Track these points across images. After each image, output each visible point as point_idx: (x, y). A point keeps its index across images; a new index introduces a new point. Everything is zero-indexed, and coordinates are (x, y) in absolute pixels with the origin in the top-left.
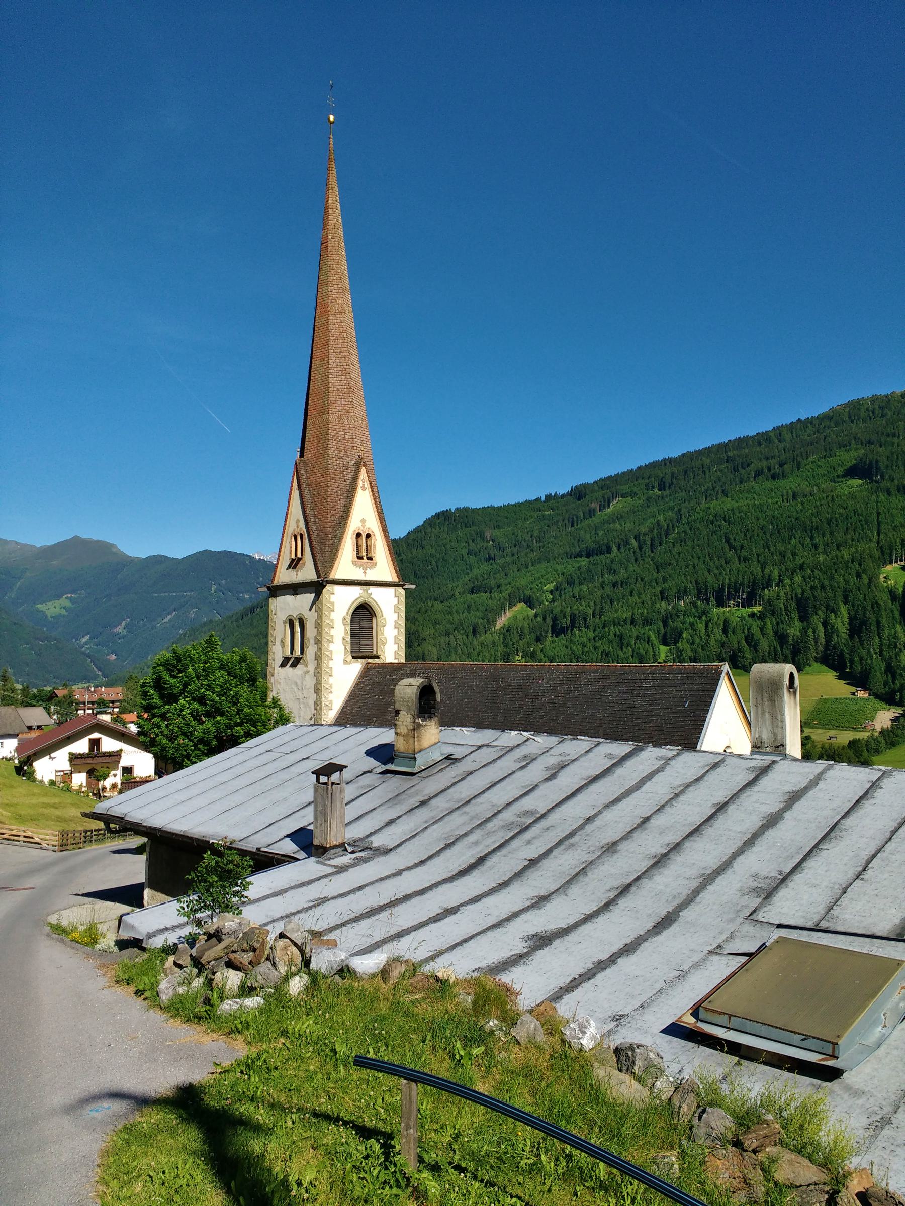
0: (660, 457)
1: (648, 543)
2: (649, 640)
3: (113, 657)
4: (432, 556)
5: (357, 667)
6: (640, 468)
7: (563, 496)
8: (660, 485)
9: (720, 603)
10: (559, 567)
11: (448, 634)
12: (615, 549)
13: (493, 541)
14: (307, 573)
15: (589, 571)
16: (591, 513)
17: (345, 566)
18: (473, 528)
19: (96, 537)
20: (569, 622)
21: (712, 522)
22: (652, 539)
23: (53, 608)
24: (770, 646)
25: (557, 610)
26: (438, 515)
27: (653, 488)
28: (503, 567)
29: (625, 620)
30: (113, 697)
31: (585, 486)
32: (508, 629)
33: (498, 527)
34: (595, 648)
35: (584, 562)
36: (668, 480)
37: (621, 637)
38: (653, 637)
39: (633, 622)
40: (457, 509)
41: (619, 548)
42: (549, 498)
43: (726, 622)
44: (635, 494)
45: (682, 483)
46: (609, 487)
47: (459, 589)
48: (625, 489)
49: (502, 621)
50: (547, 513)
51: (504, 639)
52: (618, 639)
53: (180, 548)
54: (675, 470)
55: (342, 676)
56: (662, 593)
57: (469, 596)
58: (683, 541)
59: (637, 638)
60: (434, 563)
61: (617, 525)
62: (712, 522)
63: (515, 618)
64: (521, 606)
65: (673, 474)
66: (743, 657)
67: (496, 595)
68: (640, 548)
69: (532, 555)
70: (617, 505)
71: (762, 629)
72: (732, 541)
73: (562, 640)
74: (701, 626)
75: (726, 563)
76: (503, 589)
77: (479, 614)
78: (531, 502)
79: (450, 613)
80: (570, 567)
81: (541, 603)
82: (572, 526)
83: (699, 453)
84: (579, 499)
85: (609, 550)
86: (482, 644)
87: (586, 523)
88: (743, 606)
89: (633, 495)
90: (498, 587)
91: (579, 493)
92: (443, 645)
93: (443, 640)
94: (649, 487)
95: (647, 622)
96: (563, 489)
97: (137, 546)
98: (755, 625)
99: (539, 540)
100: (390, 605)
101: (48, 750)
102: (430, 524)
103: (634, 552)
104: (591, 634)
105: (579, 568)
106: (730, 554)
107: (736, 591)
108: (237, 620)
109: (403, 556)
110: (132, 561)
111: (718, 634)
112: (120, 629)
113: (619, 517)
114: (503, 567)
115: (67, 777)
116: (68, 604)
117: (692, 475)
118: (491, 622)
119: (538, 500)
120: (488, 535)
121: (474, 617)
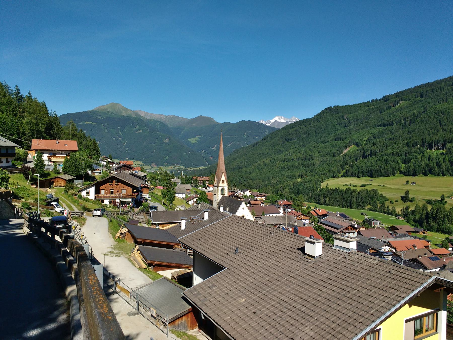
0: (424, 82)
1: (409, 122)
2: (398, 162)
3: (212, 158)
4: (323, 125)
5: (222, 196)
6: (415, 87)
7: (380, 100)
8: (421, 96)
9: (431, 148)
10: (371, 131)
11: (323, 156)
12: (395, 124)
13: (348, 119)
14: (216, 185)
15: (382, 133)
16: (390, 107)
17: (221, 184)
18: (340, 114)
19: (207, 115)
20: (369, 154)
21: (436, 114)
22: (410, 120)
23: (193, 140)
24: (446, 166)
25: (365, 149)
26: (326, 109)
27: (418, 97)
28: (349, 130)
29: (390, 154)
30: (207, 179)
31: (389, 96)
32: (346, 155)
33: (351, 113)
34: (376, 164)
35: (381, 129)
36: (425, 93)
37: (387, 160)
38: (399, 161)
39: (393, 155)
40: (334, 106)
41: (397, 123)
42: (373, 101)
43: (430, 156)
44: (410, 99)
45: (430, 95)
46: (399, 96)
47: (331, 139)
48: (406, 97)
49: (345, 152)
50: (371, 107)
51: (343, 159)
52: (385, 161)
53: (234, 120)
54: (428, 89)
55: (220, 197)
56: (407, 143)
57: (334, 142)
58: (422, 122)
59: (393, 161)
60: (323, 128)
61: (399, 113)
62: (436, 114)
63: (349, 151)
64: (353, 146)
65: (427, 91)
66: (434, 170)
67: (344, 141)
68: (405, 124)
69: (362, 126)
70: (401, 104)
71: (444, 160)
72: (442, 122)
73: (365, 160)
74: (420, 158)
75: (437, 131)
76: (347, 139)
77: (337, 149)
78: (365, 103)
79: (326, 148)
80: (376, 130)
81: (362, 145)
82: (381, 113)
83: (441, 81)
84: (386, 101)
85: (392, 124)
86: (335, 161)
87: (386, 112)
88: (440, 149)
89: (409, 100)
90: (346, 138)
91: (386, 99)
92: (321, 160)
93: (321, 158)
94: (416, 96)
95: (398, 155)
96: (379, 97)
97: (220, 119)
98: (441, 158)
99: (366, 119)
100: (226, 189)
101: (190, 200)
102: (323, 113)
103: (402, 125)
104: (376, 159)
105: (379, 132)
106: (439, 128)
107: (438, 143)
108: (251, 148)
109: (312, 125)
110: (218, 124)
111: (426, 161)
112: (214, 148)
113: (401, 109)
114: (349, 130)
115: (193, 204)
116: (198, 139)
117: (435, 92)
118: (341, 152)
119: (369, 102)
120: (345, 117)
121: (335, 150)
